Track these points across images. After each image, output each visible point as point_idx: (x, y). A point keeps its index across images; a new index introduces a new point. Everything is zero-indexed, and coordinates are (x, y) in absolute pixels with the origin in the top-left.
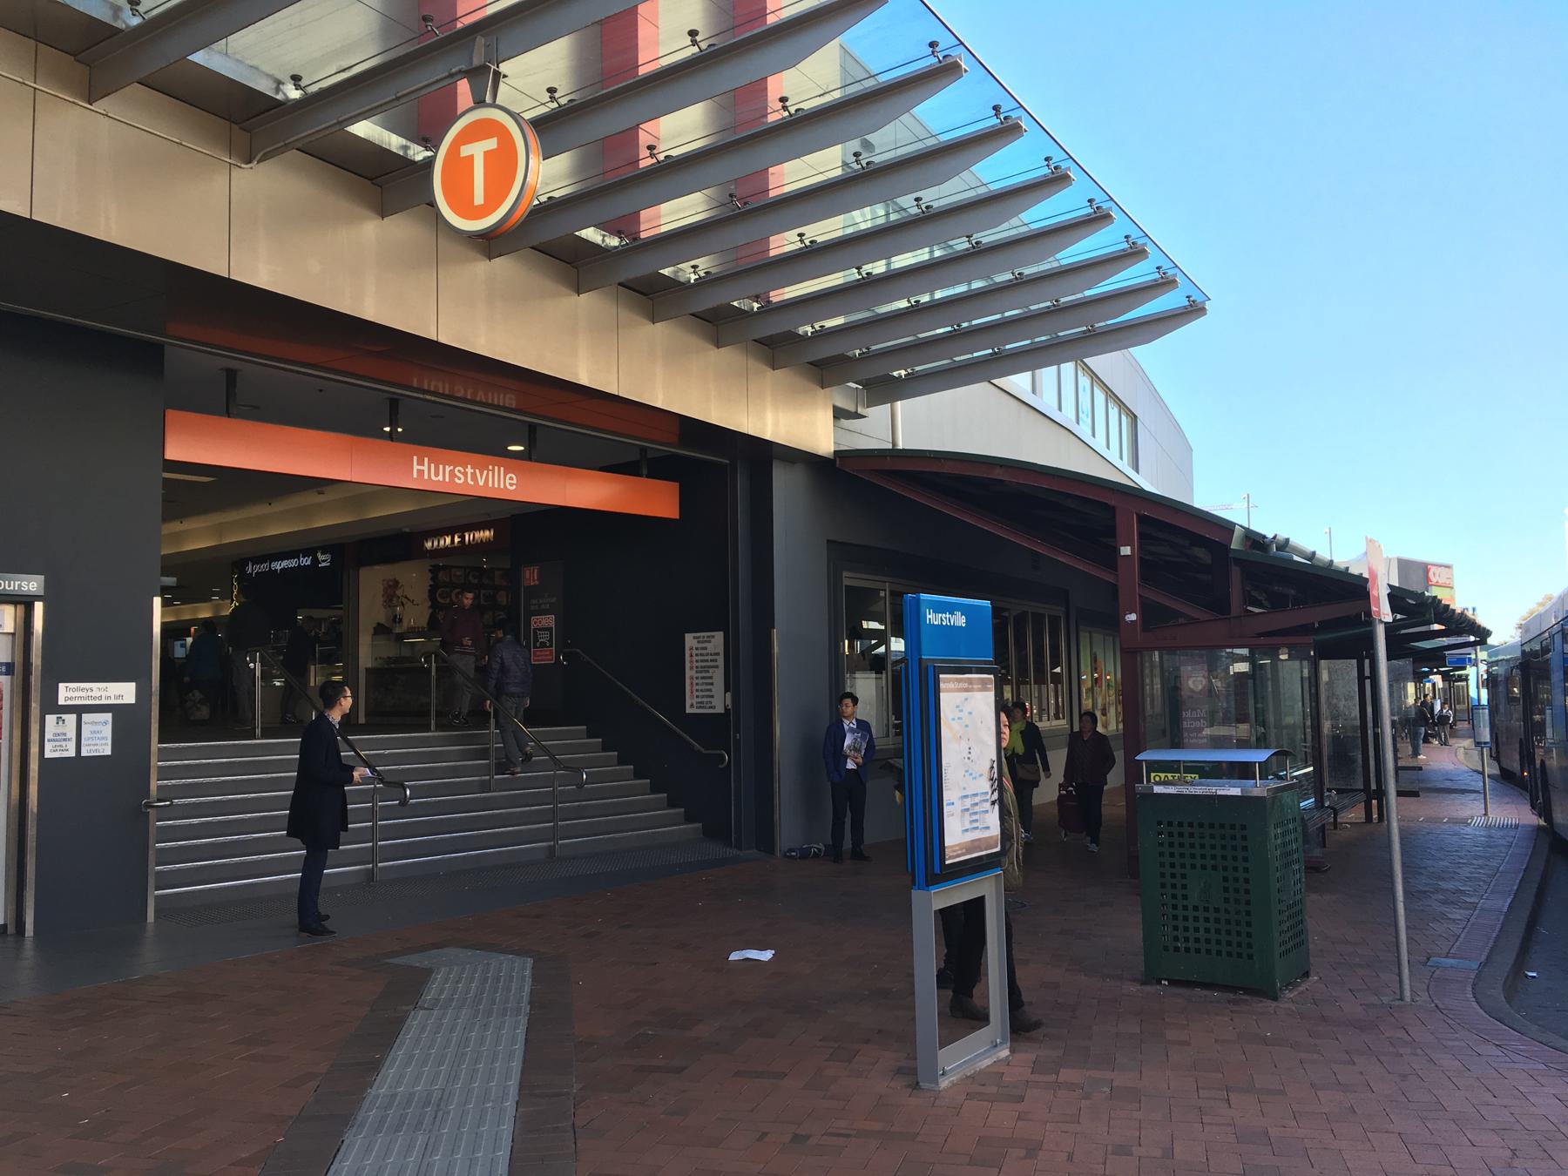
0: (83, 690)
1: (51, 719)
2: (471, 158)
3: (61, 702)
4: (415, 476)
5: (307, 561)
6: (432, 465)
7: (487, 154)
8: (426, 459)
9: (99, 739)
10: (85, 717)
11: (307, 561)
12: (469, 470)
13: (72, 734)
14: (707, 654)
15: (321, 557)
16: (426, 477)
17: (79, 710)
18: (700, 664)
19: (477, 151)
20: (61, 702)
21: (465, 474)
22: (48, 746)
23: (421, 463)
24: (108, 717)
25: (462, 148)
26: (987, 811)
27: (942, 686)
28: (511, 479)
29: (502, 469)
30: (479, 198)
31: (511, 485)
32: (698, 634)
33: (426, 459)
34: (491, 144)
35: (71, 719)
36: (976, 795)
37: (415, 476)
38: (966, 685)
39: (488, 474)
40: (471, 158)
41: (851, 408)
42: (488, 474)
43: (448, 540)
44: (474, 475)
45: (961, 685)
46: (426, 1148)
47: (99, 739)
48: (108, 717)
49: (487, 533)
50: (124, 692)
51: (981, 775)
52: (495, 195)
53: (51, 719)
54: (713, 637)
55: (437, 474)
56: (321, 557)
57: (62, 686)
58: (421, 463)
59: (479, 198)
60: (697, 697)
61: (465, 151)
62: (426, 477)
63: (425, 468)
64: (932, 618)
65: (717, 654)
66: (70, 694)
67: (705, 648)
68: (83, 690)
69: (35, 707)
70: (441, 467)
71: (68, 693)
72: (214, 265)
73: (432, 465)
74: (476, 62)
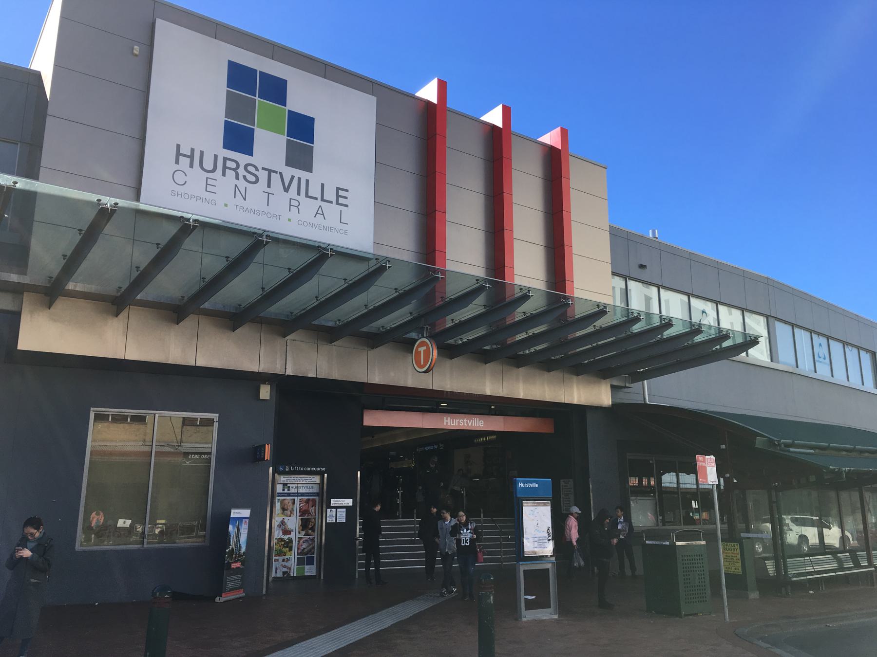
0: (337, 501)
1: (329, 510)
2: (421, 351)
3: (332, 505)
4: (445, 424)
5: (436, 447)
6: (451, 420)
7: (424, 350)
8: (449, 418)
9: (342, 516)
10: (338, 510)
11: (436, 447)
12: (465, 420)
13: (335, 516)
14: (568, 489)
15: (441, 445)
16: (449, 424)
17: (336, 508)
18: (566, 492)
19: (422, 349)
20: (332, 505)
21: (464, 422)
22: (328, 519)
23: (447, 419)
24: (345, 510)
25: (419, 349)
26: (546, 543)
27: (524, 504)
28: (482, 422)
29: (478, 419)
30: (422, 363)
31: (482, 424)
32: (565, 480)
33: (449, 418)
34: (425, 348)
35: (334, 510)
36: (541, 537)
37: (445, 424)
38: (536, 504)
39: (472, 422)
40: (421, 351)
41: (623, 385)
42: (472, 422)
43: (482, 439)
44: (467, 422)
45: (533, 504)
46: (203, 448)
47: (342, 516)
48: (345, 510)
49: (494, 437)
50: (349, 502)
51: (543, 531)
52: (426, 362)
53: (329, 510)
54: (569, 481)
55: (453, 423)
56: (441, 445)
57: (332, 500)
58: (447, 419)
59: (422, 363)
60: (565, 506)
61: (420, 349)
62: (449, 424)
63: (449, 421)
64: (521, 485)
65: (571, 489)
66: (334, 503)
67: (567, 486)
68: (337, 501)
69: (324, 506)
70: (454, 420)
71: (334, 502)
72: (363, 380)
73: (451, 420)
74: (421, 326)
